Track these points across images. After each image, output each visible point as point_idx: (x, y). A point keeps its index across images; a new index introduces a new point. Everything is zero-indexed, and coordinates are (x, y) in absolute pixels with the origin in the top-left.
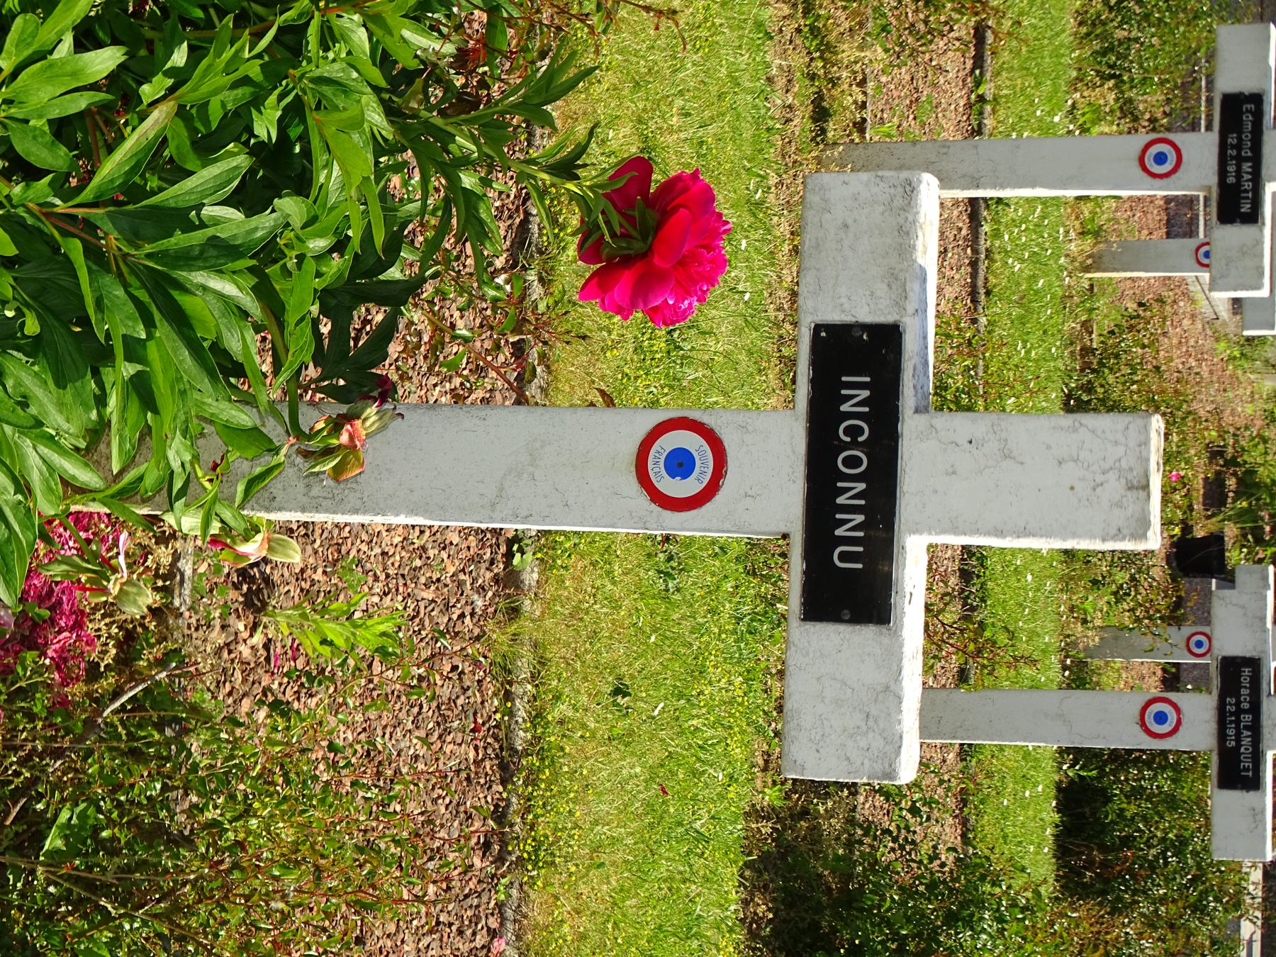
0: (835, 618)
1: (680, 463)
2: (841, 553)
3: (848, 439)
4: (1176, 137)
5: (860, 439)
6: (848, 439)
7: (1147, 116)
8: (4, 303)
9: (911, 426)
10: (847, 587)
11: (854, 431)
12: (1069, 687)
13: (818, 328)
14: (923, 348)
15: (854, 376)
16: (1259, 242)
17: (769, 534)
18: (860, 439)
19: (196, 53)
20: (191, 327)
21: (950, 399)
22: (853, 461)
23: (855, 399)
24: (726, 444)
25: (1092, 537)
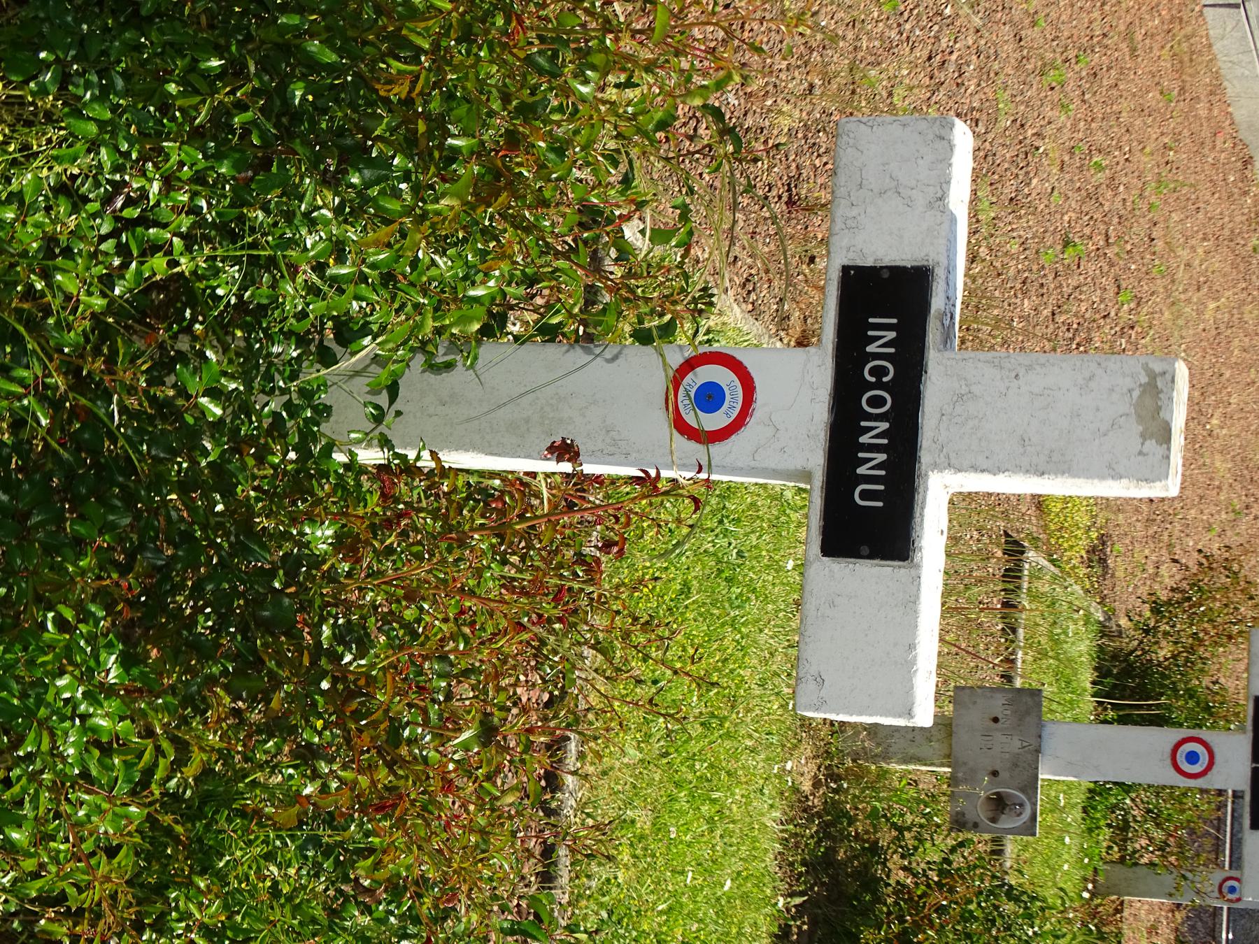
0: (897, 272)
2: (863, 492)
4: (1203, 734)
5: (885, 379)
7: (1240, 184)
8: (3, 420)
9: (936, 360)
11: (879, 372)
12: (832, 821)
13: (846, 269)
14: (952, 292)
15: (884, 314)
18: (885, 379)
21: (972, 340)
22: (876, 407)
23: (881, 341)
24: (750, 369)
25: (894, 716)
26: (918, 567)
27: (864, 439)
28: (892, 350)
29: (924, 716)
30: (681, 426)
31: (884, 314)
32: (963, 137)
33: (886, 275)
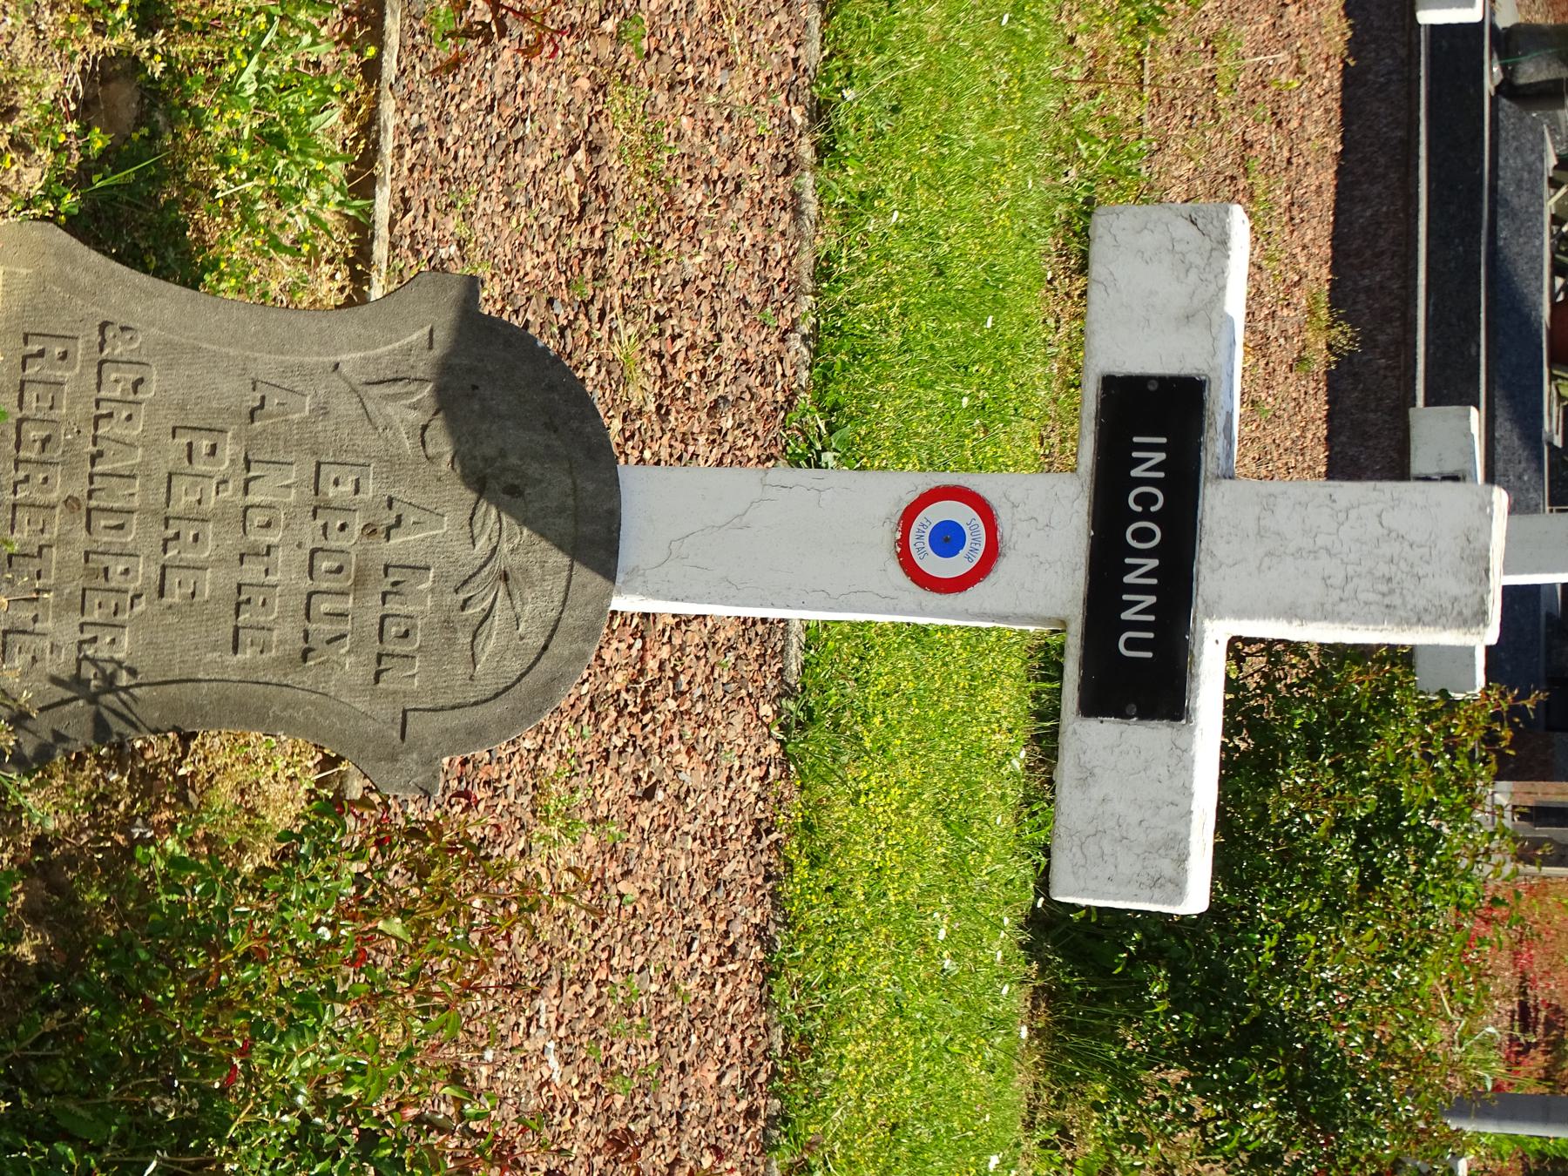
0: (1118, 711)
1: (948, 542)
3: (1139, 509)
5: (1153, 509)
6: (1139, 509)
10: (1136, 679)
13: (1110, 383)
14: (1228, 403)
15: (1150, 426)
16: (1182, 759)
17: (1033, 620)
18: (1153, 509)
19: (1034, 905)
20: (466, 301)
23: (1149, 462)
26: (1192, 731)
27: (1150, 600)
28: (1161, 475)
29: (1195, 899)
30: (910, 514)
31: (1150, 426)
32: (1238, 222)
33: (1132, 708)
